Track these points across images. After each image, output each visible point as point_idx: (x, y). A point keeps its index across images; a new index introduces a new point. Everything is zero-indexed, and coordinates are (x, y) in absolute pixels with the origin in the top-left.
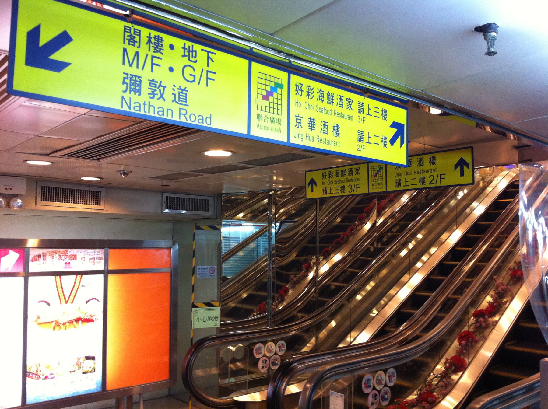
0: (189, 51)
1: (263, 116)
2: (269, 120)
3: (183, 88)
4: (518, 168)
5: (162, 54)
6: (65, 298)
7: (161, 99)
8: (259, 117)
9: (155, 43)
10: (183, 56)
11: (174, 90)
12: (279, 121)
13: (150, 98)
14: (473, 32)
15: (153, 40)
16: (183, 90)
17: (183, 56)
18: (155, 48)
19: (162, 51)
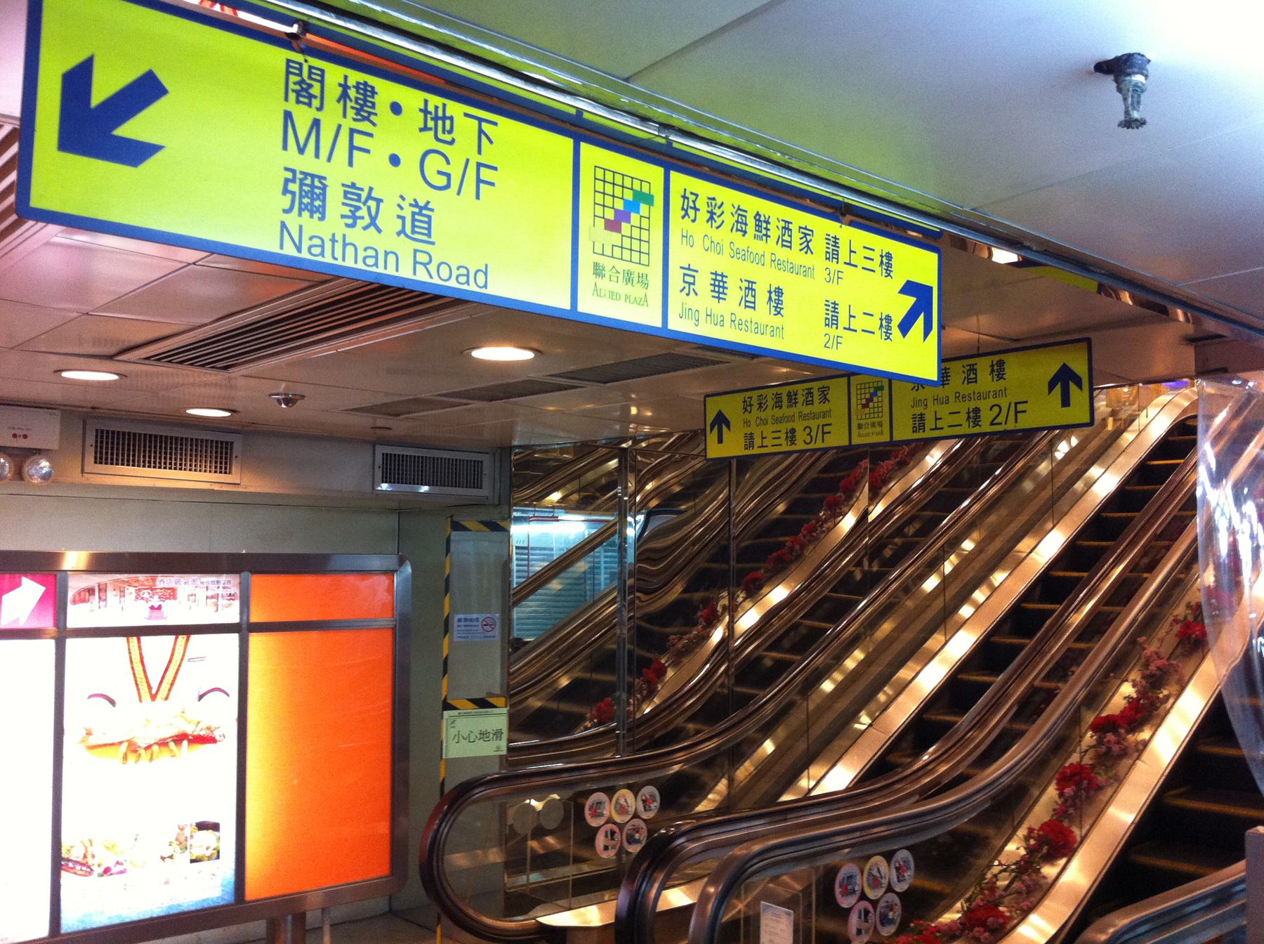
0: (436, 119)
1: (608, 268)
2: (621, 277)
3: (422, 204)
4: (1195, 389)
5: (374, 124)
6: (150, 688)
7: (372, 228)
8: (598, 270)
9: (357, 99)
10: (421, 130)
11: (401, 208)
12: (643, 280)
13: (347, 225)
14: (1090, 73)
15: (352, 93)
16: (421, 208)
17: (421, 130)
18: (358, 112)
19: (373, 118)
